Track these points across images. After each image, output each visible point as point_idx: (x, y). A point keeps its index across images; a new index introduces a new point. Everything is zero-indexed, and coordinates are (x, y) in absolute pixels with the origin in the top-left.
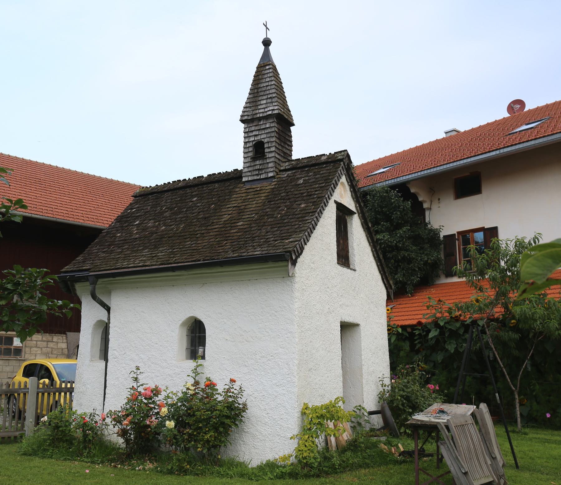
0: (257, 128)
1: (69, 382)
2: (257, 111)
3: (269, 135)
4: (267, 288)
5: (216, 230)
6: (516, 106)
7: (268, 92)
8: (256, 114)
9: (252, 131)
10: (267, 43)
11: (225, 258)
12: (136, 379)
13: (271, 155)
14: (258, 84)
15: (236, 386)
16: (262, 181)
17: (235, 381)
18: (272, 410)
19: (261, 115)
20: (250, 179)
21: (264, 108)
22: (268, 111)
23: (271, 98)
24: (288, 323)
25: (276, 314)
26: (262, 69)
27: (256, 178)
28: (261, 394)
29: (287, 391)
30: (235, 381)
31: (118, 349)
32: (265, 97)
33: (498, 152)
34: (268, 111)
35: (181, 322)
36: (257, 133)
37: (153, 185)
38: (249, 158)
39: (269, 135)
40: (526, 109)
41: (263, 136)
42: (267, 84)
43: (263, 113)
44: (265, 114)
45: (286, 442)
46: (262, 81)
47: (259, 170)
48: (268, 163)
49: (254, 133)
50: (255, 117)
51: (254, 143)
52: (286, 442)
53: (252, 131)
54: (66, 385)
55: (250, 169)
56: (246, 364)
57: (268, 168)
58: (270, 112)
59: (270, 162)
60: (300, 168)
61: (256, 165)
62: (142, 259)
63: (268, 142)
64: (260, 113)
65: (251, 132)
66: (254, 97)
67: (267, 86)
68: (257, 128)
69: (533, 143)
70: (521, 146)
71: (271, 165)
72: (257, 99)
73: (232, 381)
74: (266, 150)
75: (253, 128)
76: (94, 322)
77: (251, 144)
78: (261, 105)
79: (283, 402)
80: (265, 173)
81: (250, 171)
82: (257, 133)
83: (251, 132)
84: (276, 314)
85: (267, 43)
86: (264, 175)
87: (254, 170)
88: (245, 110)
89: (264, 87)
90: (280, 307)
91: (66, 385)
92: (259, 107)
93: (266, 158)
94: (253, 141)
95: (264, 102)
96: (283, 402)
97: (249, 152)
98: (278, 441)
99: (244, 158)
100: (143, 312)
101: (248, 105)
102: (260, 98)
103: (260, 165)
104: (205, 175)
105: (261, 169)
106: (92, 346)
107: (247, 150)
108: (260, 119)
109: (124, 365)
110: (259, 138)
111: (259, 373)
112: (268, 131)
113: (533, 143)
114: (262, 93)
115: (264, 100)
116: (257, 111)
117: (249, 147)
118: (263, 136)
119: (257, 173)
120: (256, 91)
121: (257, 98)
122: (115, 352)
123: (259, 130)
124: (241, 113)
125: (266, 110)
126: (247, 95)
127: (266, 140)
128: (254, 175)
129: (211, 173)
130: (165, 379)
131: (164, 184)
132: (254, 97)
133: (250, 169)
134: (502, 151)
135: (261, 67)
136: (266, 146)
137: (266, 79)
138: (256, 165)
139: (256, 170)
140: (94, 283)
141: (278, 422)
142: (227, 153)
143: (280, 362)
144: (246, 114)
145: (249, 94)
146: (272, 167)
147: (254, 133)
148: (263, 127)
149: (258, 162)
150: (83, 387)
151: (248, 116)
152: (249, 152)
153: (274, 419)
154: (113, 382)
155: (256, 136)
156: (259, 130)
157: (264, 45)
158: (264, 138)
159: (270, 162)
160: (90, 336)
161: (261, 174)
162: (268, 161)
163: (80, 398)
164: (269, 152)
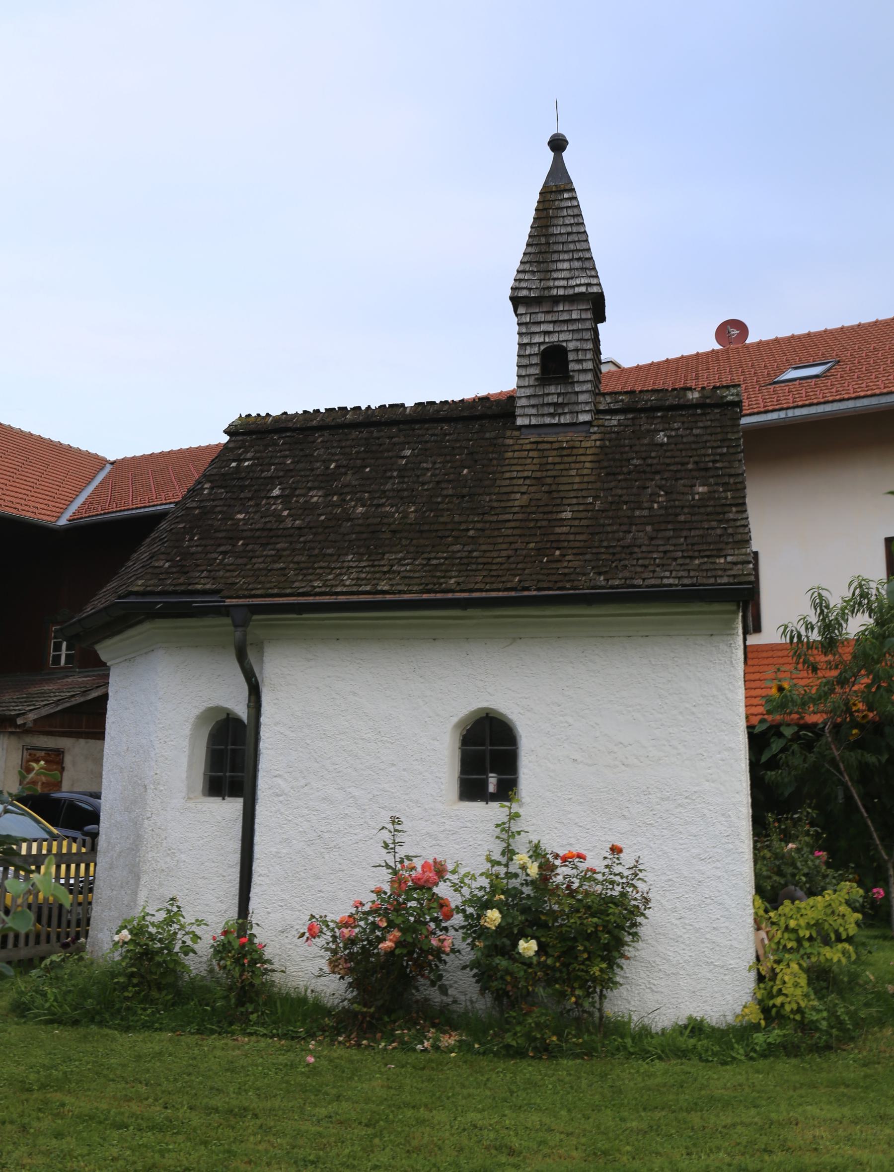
0: (549, 318)
1: (35, 841)
2: (551, 283)
3: (576, 336)
4: (672, 655)
5: (513, 524)
6: (732, 331)
7: (572, 246)
8: (549, 288)
9: (539, 323)
10: (558, 144)
11: (593, 588)
12: (637, 861)
13: (582, 377)
14: (547, 227)
15: (627, 858)
16: (561, 429)
17: (620, 851)
18: (691, 910)
19: (561, 292)
20: (534, 421)
21: (567, 279)
22: (578, 285)
23: (579, 259)
24: (723, 731)
25: (694, 710)
26: (553, 197)
27: (548, 420)
28: (664, 878)
29: (726, 872)
30: (620, 851)
31: (286, 776)
32: (566, 257)
33: (782, 414)
34: (578, 285)
35: (455, 720)
36: (550, 328)
37: (276, 412)
38: (533, 378)
39: (576, 336)
40: (751, 339)
41: (563, 337)
42: (569, 229)
43: (565, 287)
44: (571, 292)
45: (726, 978)
46: (555, 221)
47: (555, 405)
48: (577, 393)
49: (544, 327)
50: (546, 293)
51: (542, 348)
52: (726, 978)
53: (539, 323)
54: (29, 848)
55: (533, 401)
56: (625, 813)
57: (578, 403)
58: (583, 289)
59: (582, 392)
60: (643, 410)
61: (548, 394)
62: (348, 577)
63: (577, 350)
64: (558, 287)
65: (534, 323)
66: (540, 253)
67: (569, 234)
68: (549, 318)
69: (850, 404)
70: (828, 408)
71: (582, 398)
72: (548, 257)
73: (616, 850)
74: (572, 366)
75: (541, 317)
76: (197, 712)
77: (536, 350)
78: (557, 270)
79: (717, 894)
80: (571, 412)
81: (533, 406)
82: (550, 328)
83: (534, 323)
84: (694, 710)
85: (558, 144)
86: (568, 417)
87: (543, 405)
88: (521, 276)
89: (561, 234)
90: (703, 696)
91: (29, 848)
92: (555, 275)
93: (573, 383)
94: (540, 344)
95: (566, 265)
96: (717, 894)
97: (531, 365)
98: (709, 975)
99: (519, 376)
100: (354, 694)
101: (527, 267)
102: (555, 257)
103: (559, 394)
104: (409, 403)
105: (562, 405)
106: (190, 765)
107: (525, 361)
108: (557, 300)
109: (306, 811)
110: (554, 338)
111: (656, 833)
112: (575, 327)
113: (850, 404)
114: (560, 247)
115: (564, 261)
116: (551, 283)
117: (530, 355)
118: (563, 337)
119: (552, 411)
120: (543, 240)
121: (548, 256)
122: (279, 781)
123: (554, 322)
124: (511, 283)
125: (572, 282)
126: (523, 248)
127: (571, 346)
128: (543, 415)
129: (425, 401)
130: (418, 844)
131: (305, 412)
132: (540, 253)
133: (533, 401)
134: (790, 413)
135: (551, 192)
136: (571, 356)
137: (556, 218)
138: (548, 394)
139: (549, 404)
140: (241, 624)
141: (708, 936)
142: (481, 362)
143: (706, 811)
144: (524, 285)
145: (528, 245)
146: (587, 403)
147: (544, 327)
148: (565, 317)
149: (552, 389)
150: (168, 859)
151: (530, 289)
152: (531, 365)
153: (697, 930)
154: (274, 850)
155: (546, 333)
156: (554, 322)
157: (553, 149)
158: (566, 341)
159: (582, 392)
160: (186, 743)
161: (560, 415)
162: (577, 389)
163: (161, 885)
164: (579, 371)
